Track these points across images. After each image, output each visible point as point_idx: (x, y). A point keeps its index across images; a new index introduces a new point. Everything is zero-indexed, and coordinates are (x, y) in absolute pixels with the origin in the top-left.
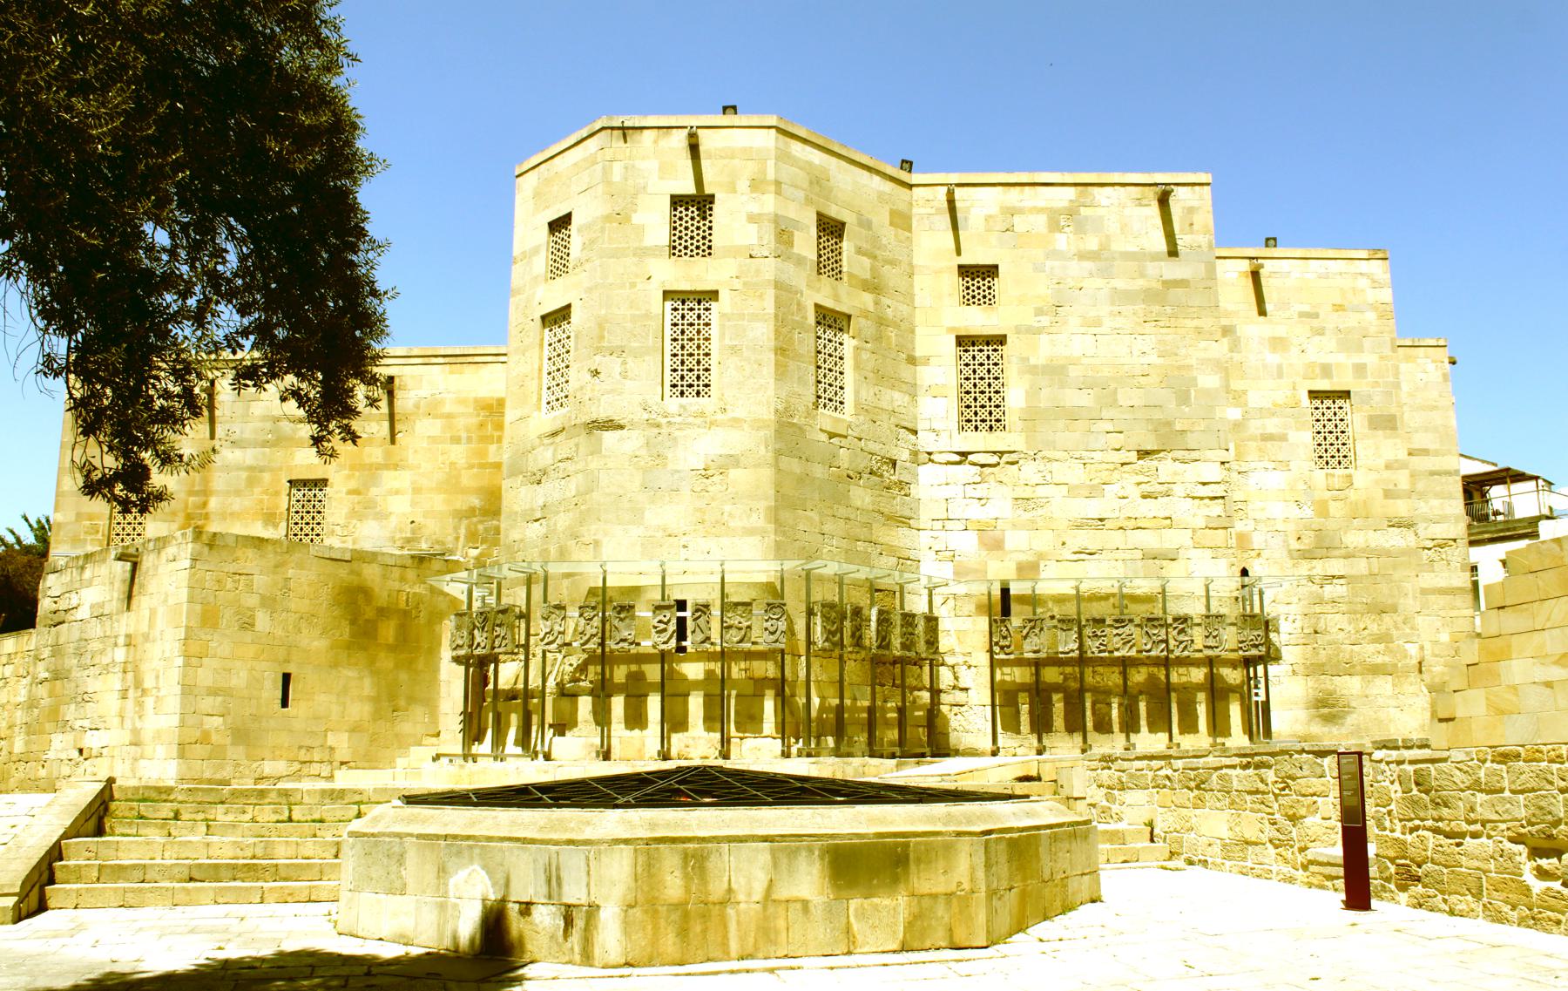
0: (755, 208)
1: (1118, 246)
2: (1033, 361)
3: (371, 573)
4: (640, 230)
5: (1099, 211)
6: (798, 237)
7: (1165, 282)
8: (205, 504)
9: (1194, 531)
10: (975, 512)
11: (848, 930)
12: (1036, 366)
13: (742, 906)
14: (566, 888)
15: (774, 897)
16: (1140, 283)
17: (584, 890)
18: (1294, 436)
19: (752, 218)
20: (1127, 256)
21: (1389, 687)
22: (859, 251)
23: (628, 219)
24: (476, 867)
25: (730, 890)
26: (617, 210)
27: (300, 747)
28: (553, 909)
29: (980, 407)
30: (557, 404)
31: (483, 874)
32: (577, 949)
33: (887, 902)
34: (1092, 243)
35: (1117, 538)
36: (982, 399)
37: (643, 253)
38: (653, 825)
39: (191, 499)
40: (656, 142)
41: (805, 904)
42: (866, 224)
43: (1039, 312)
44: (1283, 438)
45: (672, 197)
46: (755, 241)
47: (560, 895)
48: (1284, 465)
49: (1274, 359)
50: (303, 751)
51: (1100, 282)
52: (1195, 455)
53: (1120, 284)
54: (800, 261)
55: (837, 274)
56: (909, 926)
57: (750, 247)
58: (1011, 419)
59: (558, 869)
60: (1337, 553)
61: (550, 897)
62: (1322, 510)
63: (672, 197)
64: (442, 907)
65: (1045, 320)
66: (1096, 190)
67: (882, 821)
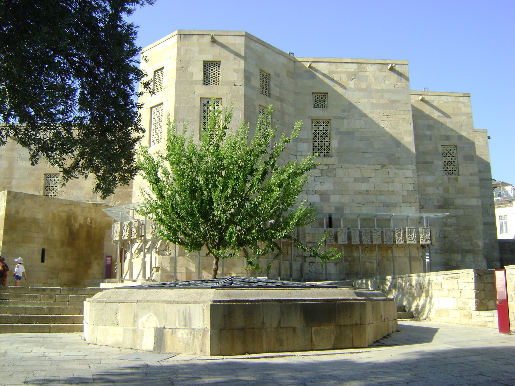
0: (236, 67)
1: (373, 87)
2: (341, 130)
3: (78, 210)
4: (192, 74)
5: (367, 74)
6: (253, 78)
7: (391, 101)
8: (11, 183)
9: (403, 196)
10: (318, 187)
11: (312, 340)
12: (342, 132)
13: (268, 329)
14: (193, 322)
15: (282, 326)
16: (381, 101)
17: (202, 323)
18: (436, 162)
19: (235, 70)
20: (376, 91)
21: (471, 257)
22: (275, 85)
23: (186, 69)
24: (152, 314)
25: (263, 323)
26: (182, 66)
27: (48, 278)
28: (187, 331)
29: (321, 147)
30: (157, 142)
31: (155, 317)
32: (198, 348)
33: (327, 328)
34: (363, 85)
35: (373, 198)
36: (321, 144)
37: (192, 83)
38: (229, 295)
39: (6, 180)
40: (198, 40)
41: (294, 329)
42: (278, 75)
43: (343, 111)
44: (432, 163)
45: (204, 61)
46: (236, 80)
47: (190, 325)
48: (433, 173)
49: (428, 133)
50: (49, 280)
51: (366, 100)
52: (402, 167)
53: (374, 101)
54: (253, 88)
55: (269, 95)
56: (336, 338)
57: (234, 82)
58: (333, 151)
59: (189, 314)
60: (452, 207)
61: (186, 326)
62: (446, 190)
63: (204, 61)
64: (134, 331)
65: (345, 114)
66: (365, 65)
67: (322, 294)
